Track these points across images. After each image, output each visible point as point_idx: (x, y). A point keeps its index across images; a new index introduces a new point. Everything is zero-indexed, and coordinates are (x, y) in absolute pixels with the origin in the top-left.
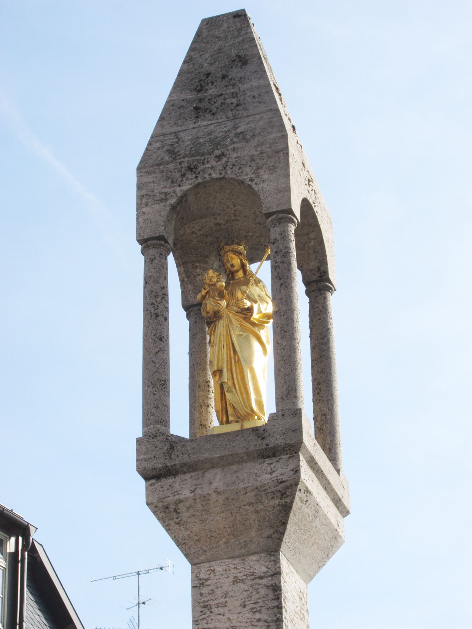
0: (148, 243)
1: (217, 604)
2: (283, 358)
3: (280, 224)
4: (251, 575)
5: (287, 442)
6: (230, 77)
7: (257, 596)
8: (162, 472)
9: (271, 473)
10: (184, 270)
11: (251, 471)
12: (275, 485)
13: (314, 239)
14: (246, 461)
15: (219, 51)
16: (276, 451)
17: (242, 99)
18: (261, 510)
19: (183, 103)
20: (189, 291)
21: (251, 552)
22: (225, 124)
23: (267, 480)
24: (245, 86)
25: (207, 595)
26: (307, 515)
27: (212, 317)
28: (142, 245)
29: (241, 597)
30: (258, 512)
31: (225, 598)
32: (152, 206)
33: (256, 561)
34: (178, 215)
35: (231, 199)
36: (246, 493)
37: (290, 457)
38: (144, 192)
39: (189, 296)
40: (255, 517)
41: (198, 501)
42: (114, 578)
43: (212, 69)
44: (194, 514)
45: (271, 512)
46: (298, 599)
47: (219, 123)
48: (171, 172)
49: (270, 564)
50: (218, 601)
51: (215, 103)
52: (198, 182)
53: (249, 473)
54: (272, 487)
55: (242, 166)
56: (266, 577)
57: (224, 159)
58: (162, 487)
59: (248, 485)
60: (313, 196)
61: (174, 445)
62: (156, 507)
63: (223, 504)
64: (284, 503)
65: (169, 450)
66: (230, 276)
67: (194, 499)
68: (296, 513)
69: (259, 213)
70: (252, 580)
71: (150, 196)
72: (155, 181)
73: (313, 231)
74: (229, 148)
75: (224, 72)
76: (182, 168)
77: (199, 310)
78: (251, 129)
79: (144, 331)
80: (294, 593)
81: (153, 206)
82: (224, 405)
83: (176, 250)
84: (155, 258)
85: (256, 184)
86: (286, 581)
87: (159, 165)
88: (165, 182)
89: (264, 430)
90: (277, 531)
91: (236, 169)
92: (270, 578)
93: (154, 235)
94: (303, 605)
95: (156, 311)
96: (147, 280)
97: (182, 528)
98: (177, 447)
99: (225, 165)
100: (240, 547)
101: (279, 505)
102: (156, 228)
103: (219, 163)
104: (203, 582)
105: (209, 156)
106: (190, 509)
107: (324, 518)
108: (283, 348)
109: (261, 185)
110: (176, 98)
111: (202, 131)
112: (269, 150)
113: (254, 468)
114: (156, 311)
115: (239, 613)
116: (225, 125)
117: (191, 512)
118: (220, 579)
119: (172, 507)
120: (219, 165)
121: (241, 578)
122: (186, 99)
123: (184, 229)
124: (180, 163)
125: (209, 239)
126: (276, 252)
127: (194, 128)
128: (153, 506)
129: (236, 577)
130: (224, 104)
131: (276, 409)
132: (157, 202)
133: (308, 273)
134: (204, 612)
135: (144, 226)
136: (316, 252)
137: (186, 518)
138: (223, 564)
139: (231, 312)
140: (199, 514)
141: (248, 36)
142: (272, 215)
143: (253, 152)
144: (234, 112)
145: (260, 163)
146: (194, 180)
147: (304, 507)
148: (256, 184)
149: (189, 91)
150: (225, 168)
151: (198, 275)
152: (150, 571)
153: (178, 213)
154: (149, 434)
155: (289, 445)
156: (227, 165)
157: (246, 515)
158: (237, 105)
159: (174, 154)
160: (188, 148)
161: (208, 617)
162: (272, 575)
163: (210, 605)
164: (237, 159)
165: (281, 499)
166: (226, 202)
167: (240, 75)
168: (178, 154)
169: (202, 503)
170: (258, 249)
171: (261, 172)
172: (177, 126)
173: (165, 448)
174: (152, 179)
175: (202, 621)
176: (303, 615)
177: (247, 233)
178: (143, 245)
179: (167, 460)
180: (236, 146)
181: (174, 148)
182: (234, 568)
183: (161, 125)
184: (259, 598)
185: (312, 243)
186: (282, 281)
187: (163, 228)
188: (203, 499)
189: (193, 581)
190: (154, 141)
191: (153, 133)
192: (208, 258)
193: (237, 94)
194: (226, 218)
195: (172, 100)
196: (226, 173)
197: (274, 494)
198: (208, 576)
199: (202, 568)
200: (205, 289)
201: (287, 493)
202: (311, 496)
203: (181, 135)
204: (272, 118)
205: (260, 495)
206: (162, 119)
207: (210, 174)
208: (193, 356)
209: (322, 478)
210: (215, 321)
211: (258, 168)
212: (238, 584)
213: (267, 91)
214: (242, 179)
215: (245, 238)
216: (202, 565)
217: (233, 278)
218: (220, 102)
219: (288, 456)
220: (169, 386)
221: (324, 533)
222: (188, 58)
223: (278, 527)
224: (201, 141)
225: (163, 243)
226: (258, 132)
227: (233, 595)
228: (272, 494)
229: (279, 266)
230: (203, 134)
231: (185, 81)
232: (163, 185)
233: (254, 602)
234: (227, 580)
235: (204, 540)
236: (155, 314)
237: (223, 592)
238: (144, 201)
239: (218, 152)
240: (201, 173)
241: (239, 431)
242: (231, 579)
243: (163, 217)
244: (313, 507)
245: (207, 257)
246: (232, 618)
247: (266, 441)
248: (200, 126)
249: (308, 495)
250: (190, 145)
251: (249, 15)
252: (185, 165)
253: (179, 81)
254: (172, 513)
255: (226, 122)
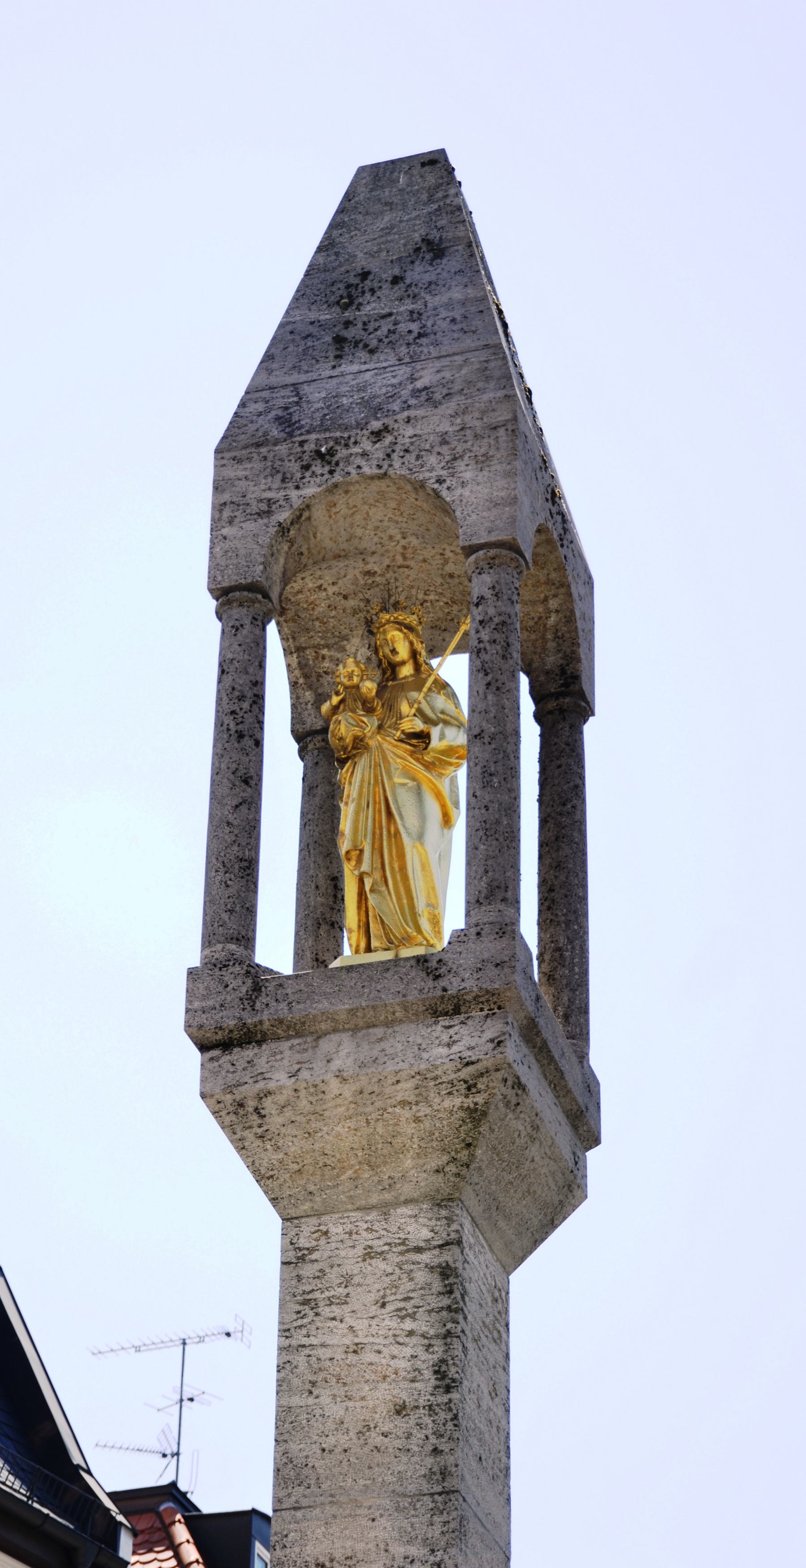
0: (230, 595)
1: (329, 1299)
2: (483, 824)
3: (491, 568)
4: (400, 1244)
5: (484, 986)
6: (408, 281)
7: (410, 1285)
8: (236, 1035)
9: (449, 1045)
10: (299, 663)
11: (410, 1039)
12: (455, 1069)
13: (557, 611)
14: (401, 1021)
15: (388, 230)
16: (461, 1002)
17: (429, 324)
18: (426, 1116)
19: (313, 329)
20: (306, 704)
21: (402, 1198)
22: (392, 371)
23: (441, 1057)
24: (437, 298)
25: (311, 1280)
26: (517, 1134)
27: (350, 748)
28: (217, 600)
29: (377, 1286)
30: (420, 1121)
31: (346, 1287)
32: (242, 524)
33: (410, 1217)
34: (292, 545)
35: (397, 522)
36: (398, 1082)
37: (487, 1016)
38: (226, 497)
39: (306, 713)
40: (413, 1131)
41: (303, 1093)
42: (138, 1349)
43: (373, 265)
44: (293, 1119)
45: (444, 1122)
46: (489, 1300)
47: (380, 369)
48: (282, 460)
49: (439, 1223)
50: (332, 1293)
51: (376, 330)
52: (333, 480)
53: (406, 1043)
54: (449, 1072)
55: (423, 453)
56: (430, 1249)
57: (389, 439)
58: (233, 1065)
59: (401, 1066)
60: (559, 526)
61: (261, 984)
62: (219, 1102)
63: (351, 1102)
64: (472, 1106)
65: (250, 993)
66: (389, 673)
67: (296, 1090)
68: (494, 1127)
69: (451, 555)
70: (402, 1253)
71: (239, 505)
72: (250, 477)
73: (555, 596)
74: (398, 417)
75: (396, 271)
76: (304, 452)
77: (323, 740)
78: (444, 381)
79: (213, 764)
80: (482, 1287)
81: (243, 525)
82: (363, 918)
83: (286, 621)
84: (242, 626)
85: (448, 488)
86: (468, 1259)
87: (258, 445)
88: (270, 479)
89: (440, 961)
90: (455, 1159)
91: (411, 458)
92: (436, 1252)
93: (243, 581)
94: (499, 1313)
95: (240, 727)
96: (225, 668)
97: (269, 1147)
98: (266, 987)
99: (389, 450)
100: (380, 1187)
101: (461, 1108)
102: (248, 567)
103: (377, 445)
104: (304, 1254)
105: (359, 432)
106: (285, 1110)
107: (549, 1143)
108: (486, 806)
109: (459, 491)
110: (298, 318)
111: (347, 383)
112: (478, 423)
113: (416, 1034)
114: (240, 727)
115: (373, 1318)
116: (394, 374)
117: (287, 1114)
118: (337, 1249)
119: (251, 1104)
120: (378, 451)
121: (379, 1250)
122: (319, 321)
123: (303, 579)
124: (302, 443)
125: (352, 603)
126: (481, 622)
127: (331, 377)
128: (213, 1101)
129: (371, 1247)
130: (394, 332)
131: (466, 923)
132: (253, 517)
133: (542, 678)
134: (303, 1313)
135: (223, 564)
136: (558, 637)
137: (278, 1127)
138: (345, 1220)
139: (387, 741)
140: (304, 1120)
141: (448, 201)
142: (477, 551)
143: (445, 426)
144: (412, 348)
145: (459, 449)
146: (327, 476)
147: (510, 1116)
148: (448, 488)
149: (325, 306)
150: (389, 456)
151: (326, 673)
152: (207, 1339)
153: (292, 542)
154: (213, 961)
155: (487, 992)
156: (393, 451)
157: (396, 1125)
158: (420, 335)
159: (289, 426)
160: (318, 415)
161: (310, 1323)
162: (441, 1246)
163: (315, 1300)
164: (415, 439)
165: (467, 1096)
166: (389, 527)
167: (427, 278)
168: (297, 425)
169: (310, 1099)
170: (445, 630)
171: (460, 465)
172: (299, 372)
173: (244, 989)
174: (244, 473)
175: (299, 1331)
176: (499, 1332)
177: (425, 594)
178: (220, 600)
179: (246, 1011)
180: (412, 413)
181: (290, 414)
182: (367, 1229)
183: (267, 370)
184: (413, 1291)
185: (553, 619)
186: (489, 678)
187: (261, 567)
188: (312, 1090)
189: (284, 1251)
190: (250, 399)
191: (249, 385)
192: (347, 640)
193: (421, 314)
194: (387, 562)
195: (290, 322)
196: (390, 466)
197: (453, 1085)
198: (314, 1243)
199: (304, 1227)
200: (337, 693)
201: (479, 1086)
202: (525, 1097)
203: (306, 389)
204: (487, 361)
205: (425, 1087)
206: (268, 357)
207: (359, 467)
208: (307, 827)
209: (549, 1064)
210: (355, 755)
211: (455, 459)
212: (373, 1261)
213: (481, 309)
214: (421, 478)
215: (422, 604)
216: (303, 1220)
217: (394, 676)
218: (384, 330)
219: (486, 1012)
220: (258, 871)
221: (548, 1174)
222: (326, 243)
223: (457, 1152)
224: (345, 402)
225: (260, 597)
226: (457, 387)
227: (362, 1281)
228: (450, 1086)
229: (485, 649)
230: (348, 389)
231: (320, 286)
232: (265, 484)
233: (402, 1297)
234: (351, 1253)
235: (311, 1172)
236: (236, 731)
237: (342, 1276)
238: (227, 513)
239: (376, 425)
240: (341, 464)
241: (389, 961)
242: (359, 1251)
243: (262, 547)
244: (528, 1120)
245: (345, 638)
246: (357, 1328)
247: (443, 983)
248: (342, 375)
249: (520, 1092)
250: (323, 408)
251: (453, 161)
252: (310, 447)
253: (307, 286)
254: (249, 1115)
255: (396, 368)
